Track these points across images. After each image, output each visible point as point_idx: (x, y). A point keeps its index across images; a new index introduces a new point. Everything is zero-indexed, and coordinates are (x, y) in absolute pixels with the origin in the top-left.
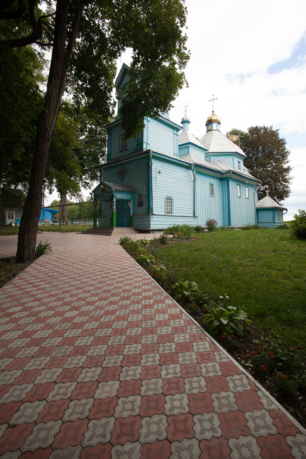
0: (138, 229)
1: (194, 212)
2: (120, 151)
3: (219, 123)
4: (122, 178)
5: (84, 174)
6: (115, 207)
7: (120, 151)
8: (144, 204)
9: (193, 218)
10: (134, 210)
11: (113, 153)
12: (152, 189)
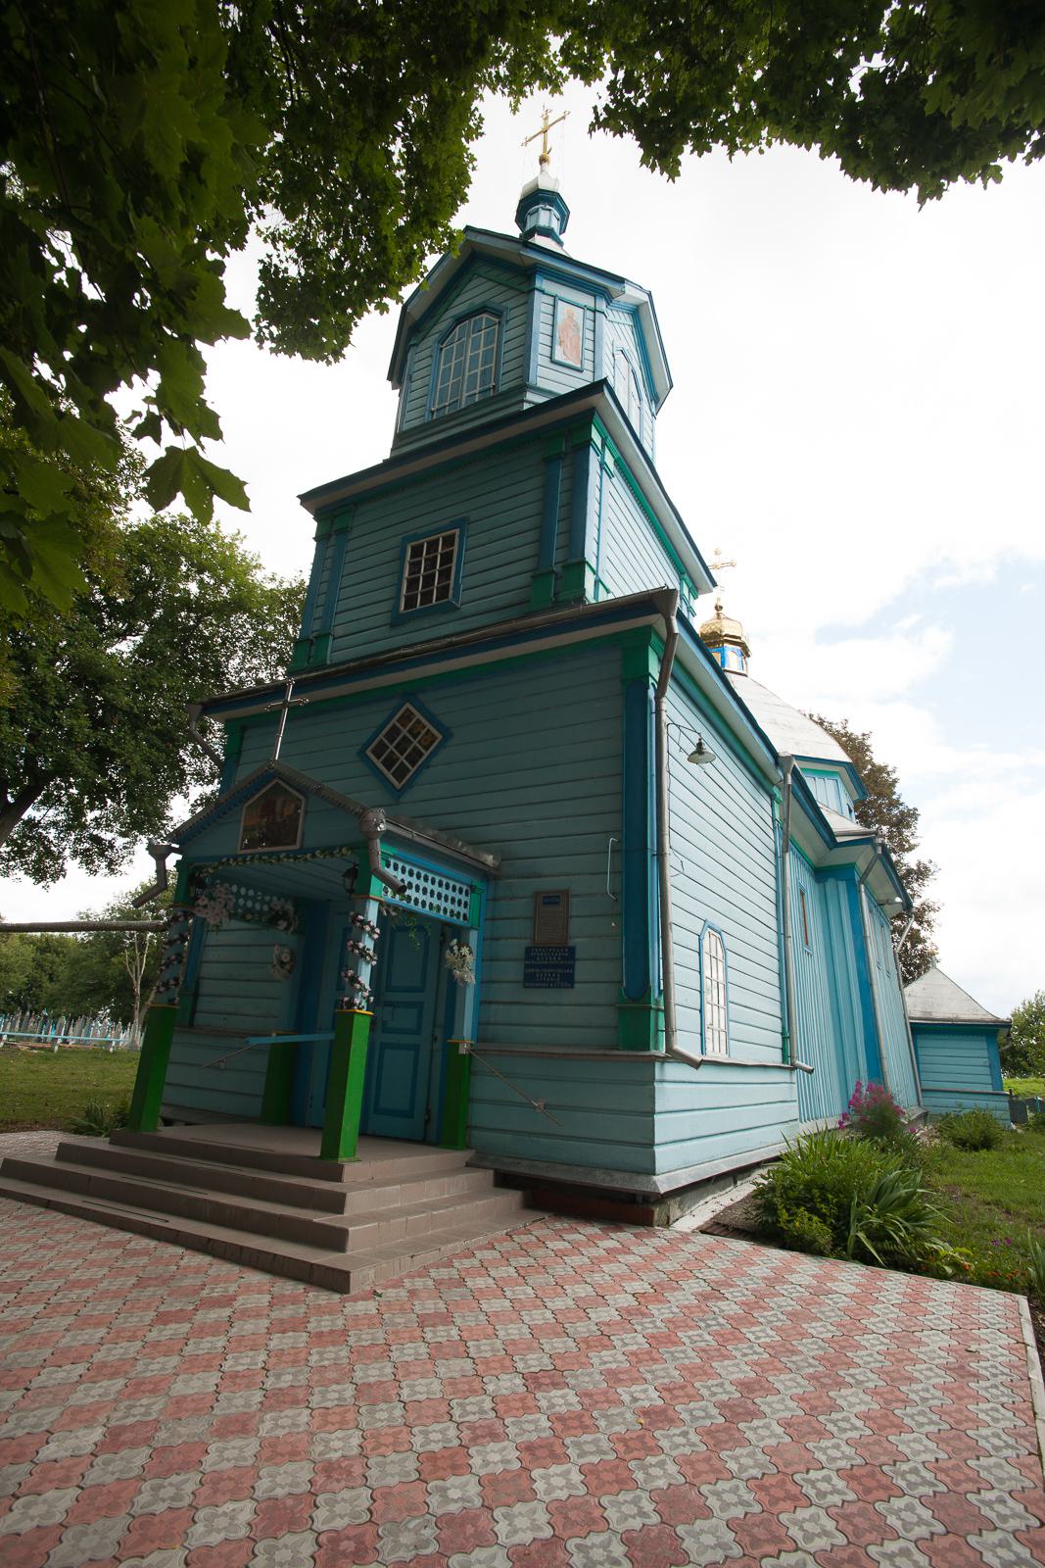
0: (523, 1169)
1: (786, 1036)
2: (397, 622)
3: (745, 652)
4: (400, 774)
5: (97, 796)
6: (365, 976)
7: (397, 622)
8: (581, 971)
9: (784, 1076)
10: (483, 1003)
11: (339, 631)
12: (661, 855)
